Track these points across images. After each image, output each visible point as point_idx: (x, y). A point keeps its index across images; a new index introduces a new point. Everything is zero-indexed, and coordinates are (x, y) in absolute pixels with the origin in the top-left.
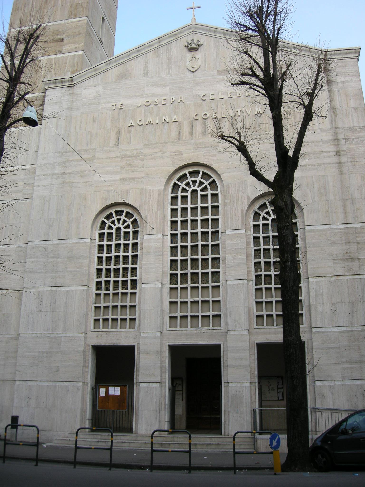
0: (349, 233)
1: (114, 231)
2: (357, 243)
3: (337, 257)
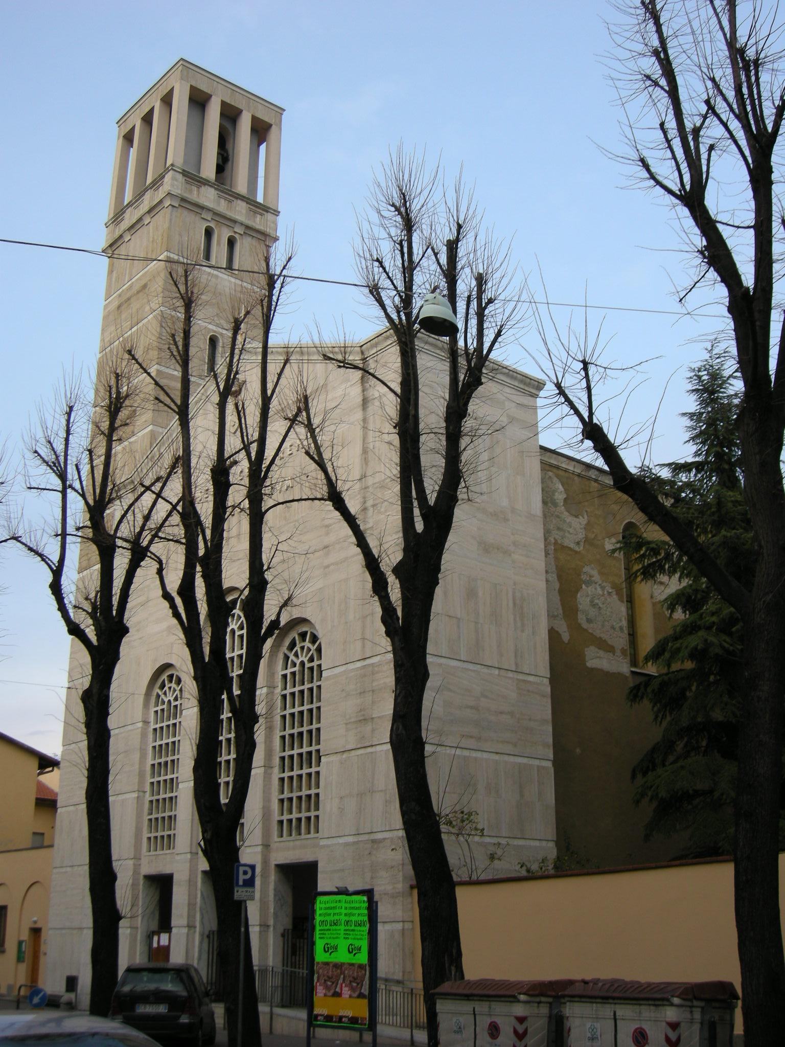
0: (365, 676)
2: (373, 691)
3: (350, 718)
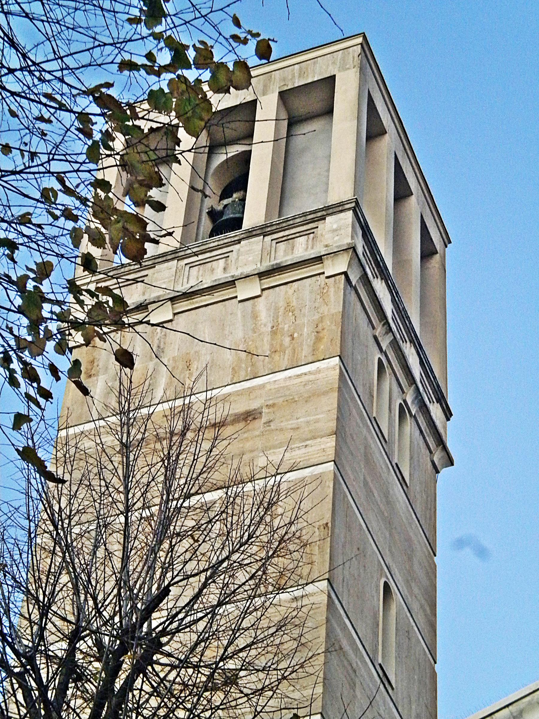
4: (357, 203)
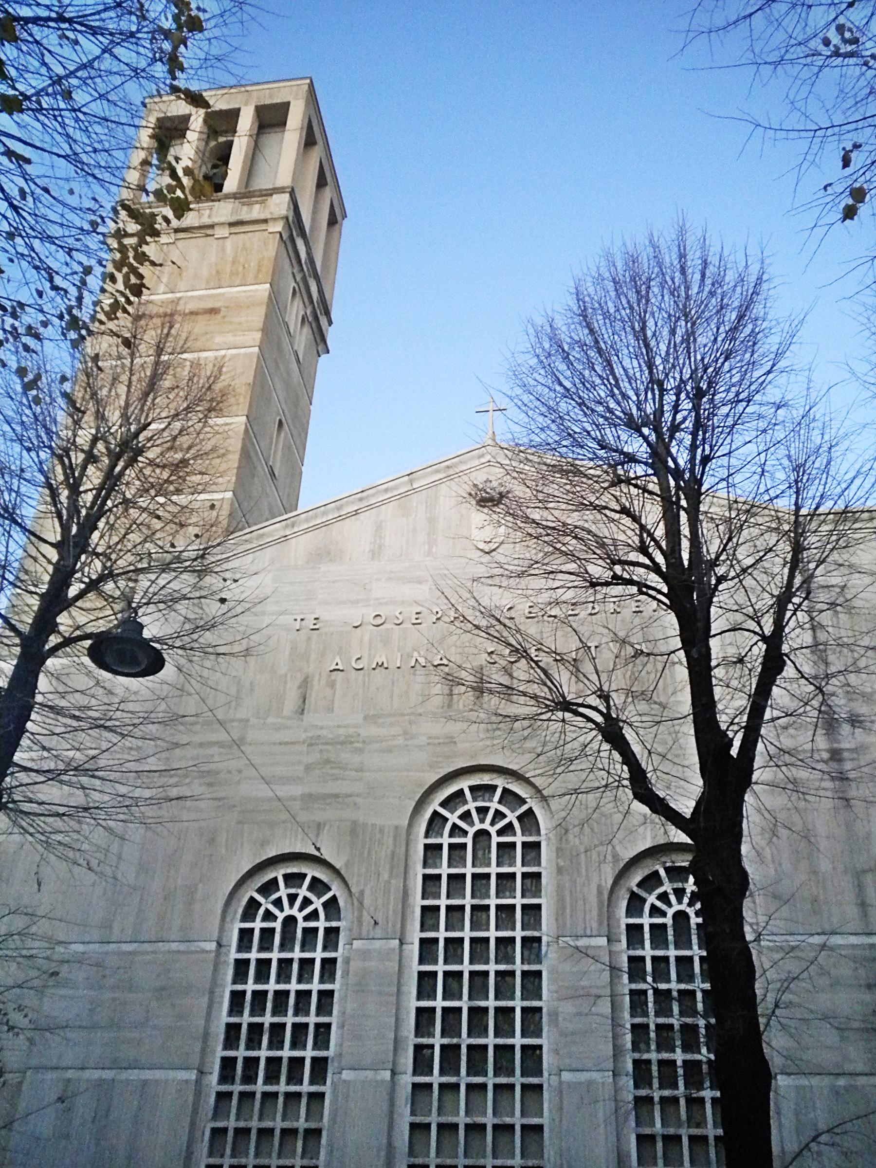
1: (278, 925)
4: (293, 189)
